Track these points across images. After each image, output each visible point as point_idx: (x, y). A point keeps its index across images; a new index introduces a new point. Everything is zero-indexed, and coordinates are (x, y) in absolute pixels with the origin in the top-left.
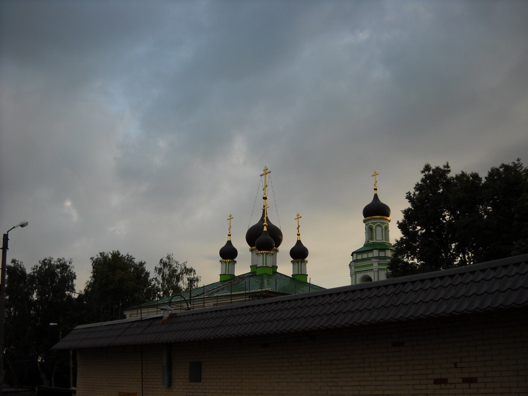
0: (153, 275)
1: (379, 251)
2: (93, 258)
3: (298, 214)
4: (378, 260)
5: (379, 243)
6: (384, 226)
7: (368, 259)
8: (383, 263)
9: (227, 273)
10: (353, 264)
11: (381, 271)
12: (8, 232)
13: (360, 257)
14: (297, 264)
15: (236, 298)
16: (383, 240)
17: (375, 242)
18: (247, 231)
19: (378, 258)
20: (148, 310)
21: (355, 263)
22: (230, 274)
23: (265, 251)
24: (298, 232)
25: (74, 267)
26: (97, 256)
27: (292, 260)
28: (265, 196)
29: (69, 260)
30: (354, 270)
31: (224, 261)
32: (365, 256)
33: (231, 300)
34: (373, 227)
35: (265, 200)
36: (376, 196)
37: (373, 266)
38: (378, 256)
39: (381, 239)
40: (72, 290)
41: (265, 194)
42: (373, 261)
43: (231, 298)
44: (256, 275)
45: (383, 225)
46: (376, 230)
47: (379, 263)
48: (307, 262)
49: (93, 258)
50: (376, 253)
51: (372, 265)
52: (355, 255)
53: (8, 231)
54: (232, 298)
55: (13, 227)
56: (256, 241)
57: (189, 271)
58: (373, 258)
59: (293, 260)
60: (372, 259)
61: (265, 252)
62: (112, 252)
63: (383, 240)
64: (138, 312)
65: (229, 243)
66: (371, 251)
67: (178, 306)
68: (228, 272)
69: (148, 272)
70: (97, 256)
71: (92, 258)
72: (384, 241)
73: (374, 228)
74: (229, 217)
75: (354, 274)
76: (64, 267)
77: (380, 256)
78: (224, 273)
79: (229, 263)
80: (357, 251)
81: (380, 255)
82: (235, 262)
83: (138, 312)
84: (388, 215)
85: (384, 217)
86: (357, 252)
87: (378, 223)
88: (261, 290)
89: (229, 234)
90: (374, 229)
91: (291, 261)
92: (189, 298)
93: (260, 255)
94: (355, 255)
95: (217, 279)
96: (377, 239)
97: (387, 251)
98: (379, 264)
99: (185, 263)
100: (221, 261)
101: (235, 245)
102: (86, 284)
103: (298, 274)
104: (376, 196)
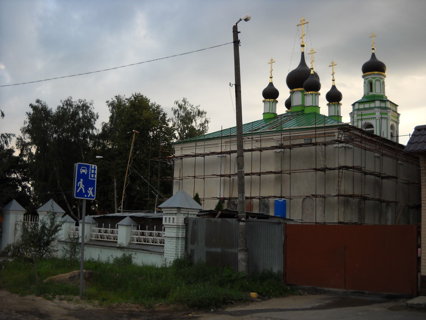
0: (170, 115)
1: (358, 104)
2: (109, 101)
3: (333, 62)
4: (380, 110)
5: (378, 96)
6: (382, 81)
7: (370, 108)
8: (384, 112)
9: (271, 112)
10: (356, 112)
11: (384, 119)
12: (237, 24)
13: (362, 106)
14: (334, 106)
15: (187, 149)
16: (381, 93)
17: (375, 94)
18: (288, 74)
19: (380, 107)
20: (290, 128)
21: (357, 112)
22: (273, 113)
23: (312, 92)
24: (333, 78)
25: (94, 108)
26: (112, 99)
27: (327, 103)
28: (302, 44)
29: (90, 101)
30: (357, 118)
31: (269, 100)
32: (367, 106)
33: (316, 131)
34: (373, 81)
35: (303, 47)
36: (373, 55)
37: (375, 114)
38: (379, 106)
39: (380, 92)
40: (93, 128)
41: (303, 42)
42: (375, 110)
43: (316, 131)
44: (305, 114)
45: (381, 80)
46: (375, 84)
47: (381, 112)
48: (341, 104)
49: (109, 101)
50: (378, 104)
51: (375, 114)
52: (357, 105)
53: (236, 23)
54: (317, 130)
55: (239, 20)
56: (305, 81)
57: (200, 113)
58: (375, 107)
59: (328, 103)
60: (374, 109)
61: (314, 93)
62: (135, 94)
63: (381, 93)
64: (196, 144)
65: (271, 84)
66: (373, 101)
67: (249, 138)
68: (272, 111)
69: (166, 113)
70: (112, 99)
71: (107, 102)
72: (382, 94)
73: (374, 82)
74: (271, 61)
75: (356, 121)
76: (85, 107)
77: (359, 109)
78: (268, 112)
79: (273, 102)
80: (359, 101)
81: (381, 106)
82: (277, 102)
83: (196, 144)
84: (384, 71)
85: (382, 73)
86: (359, 102)
87: (378, 78)
88: (324, 125)
89: (271, 76)
90: (374, 83)
91: (286, 111)
92: (236, 134)
93: (266, 103)
94: (357, 105)
95: (261, 117)
96: (376, 92)
97: (387, 102)
98: (381, 114)
99: (198, 107)
100: (264, 101)
101: (276, 86)
102: (102, 125)
103: (335, 116)
104: (373, 55)
